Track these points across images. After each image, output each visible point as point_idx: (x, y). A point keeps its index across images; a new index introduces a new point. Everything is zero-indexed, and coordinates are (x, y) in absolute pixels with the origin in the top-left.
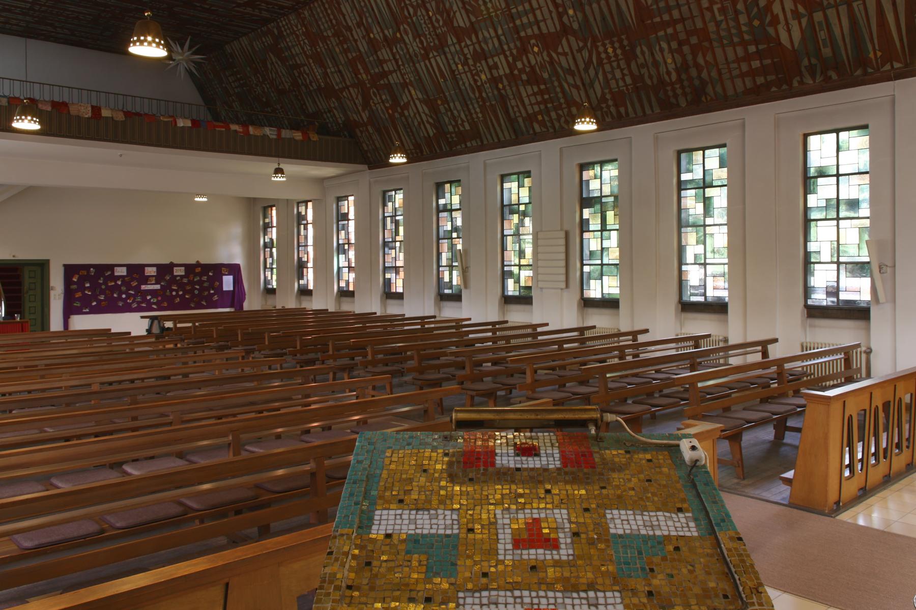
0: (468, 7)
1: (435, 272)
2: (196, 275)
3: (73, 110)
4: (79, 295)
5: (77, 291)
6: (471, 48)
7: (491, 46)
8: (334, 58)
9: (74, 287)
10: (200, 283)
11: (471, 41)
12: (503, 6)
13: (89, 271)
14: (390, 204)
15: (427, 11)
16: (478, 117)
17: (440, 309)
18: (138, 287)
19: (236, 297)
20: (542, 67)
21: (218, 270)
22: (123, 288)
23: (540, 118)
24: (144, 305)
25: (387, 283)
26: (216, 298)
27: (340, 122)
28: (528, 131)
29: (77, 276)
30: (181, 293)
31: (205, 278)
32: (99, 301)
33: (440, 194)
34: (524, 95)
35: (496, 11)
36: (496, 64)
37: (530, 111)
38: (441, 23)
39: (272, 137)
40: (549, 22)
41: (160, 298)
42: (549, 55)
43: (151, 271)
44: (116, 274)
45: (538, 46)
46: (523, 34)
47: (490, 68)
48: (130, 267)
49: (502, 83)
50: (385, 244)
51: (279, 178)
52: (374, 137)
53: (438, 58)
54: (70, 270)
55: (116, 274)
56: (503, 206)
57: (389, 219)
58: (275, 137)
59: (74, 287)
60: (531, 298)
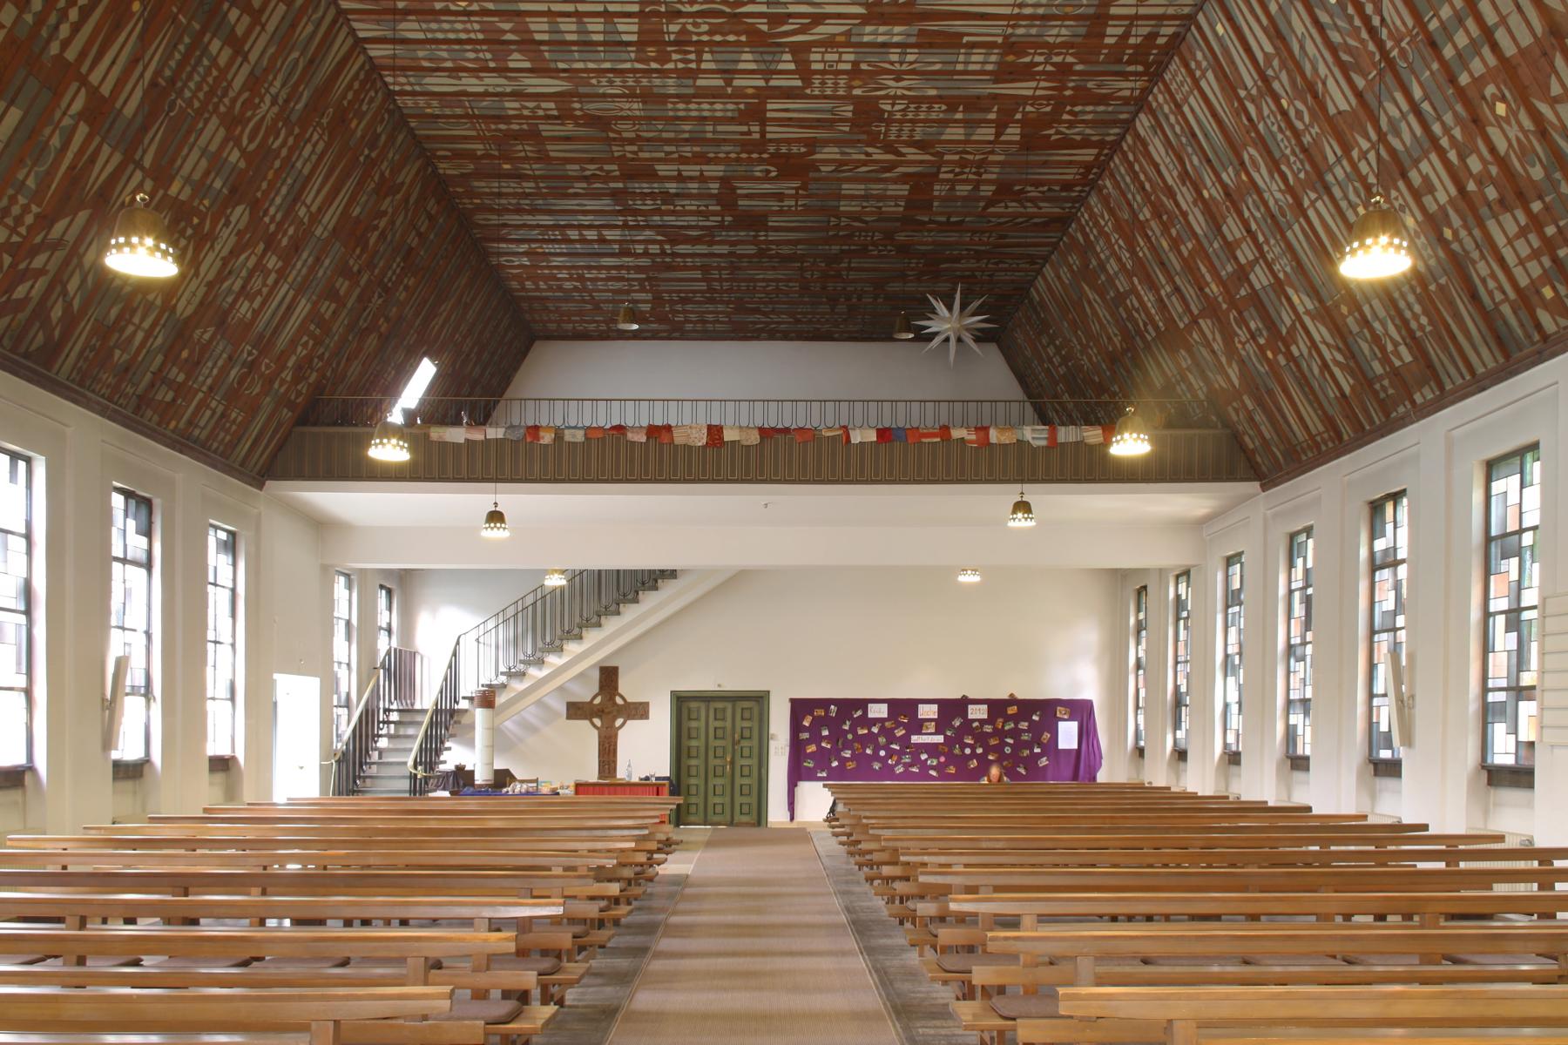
0: (1345, 57)
1: (1361, 709)
2: (1008, 718)
3: (679, 438)
4: (812, 748)
5: (809, 742)
6: (1372, 156)
7: (1407, 137)
8: (1162, 264)
9: (805, 736)
10: (1015, 733)
11: (1369, 139)
12: (1410, 22)
13: (827, 711)
14: (1299, 562)
15: (1276, 98)
16: (1422, 328)
17: (1373, 796)
18: (907, 737)
19: (1085, 759)
20: (1525, 153)
21: (1046, 711)
22: (882, 740)
23: (1548, 292)
24: (915, 770)
25: (1291, 735)
26: (1044, 762)
27: (1202, 397)
28: (1529, 337)
29: (809, 718)
30: (979, 751)
31: (1024, 725)
32: (843, 761)
33: (1378, 528)
34: (1500, 240)
35: (1398, 42)
36: (1426, 178)
37: (1524, 282)
38: (1307, 119)
39: (1036, 443)
40: (1515, 20)
41: (942, 759)
42: (1536, 116)
43: (928, 712)
44: (871, 715)
45: (1503, 99)
46: (1464, 79)
47: (1417, 195)
48: (894, 705)
49: (1450, 226)
50: (1290, 648)
51: (1020, 522)
52: (1257, 418)
53: (1319, 204)
54: (800, 708)
55: (871, 715)
56: (1488, 539)
57: (1297, 595)
58: (1044, 443)
59: (805, 736)
60: (1530, 772)
